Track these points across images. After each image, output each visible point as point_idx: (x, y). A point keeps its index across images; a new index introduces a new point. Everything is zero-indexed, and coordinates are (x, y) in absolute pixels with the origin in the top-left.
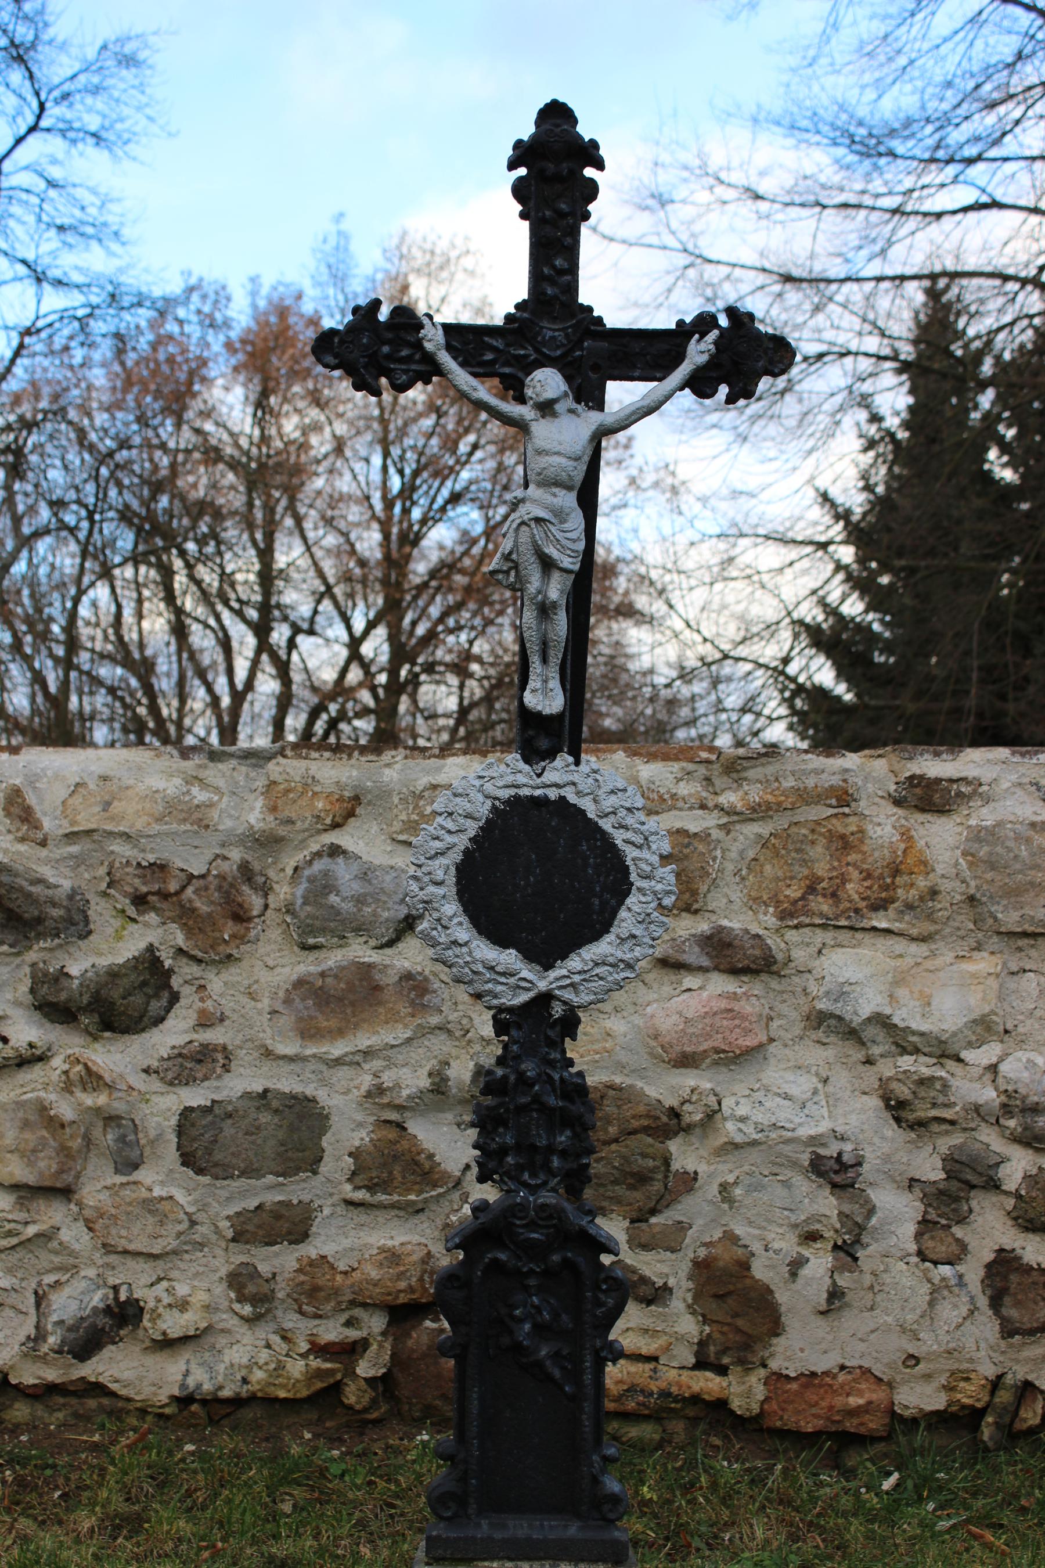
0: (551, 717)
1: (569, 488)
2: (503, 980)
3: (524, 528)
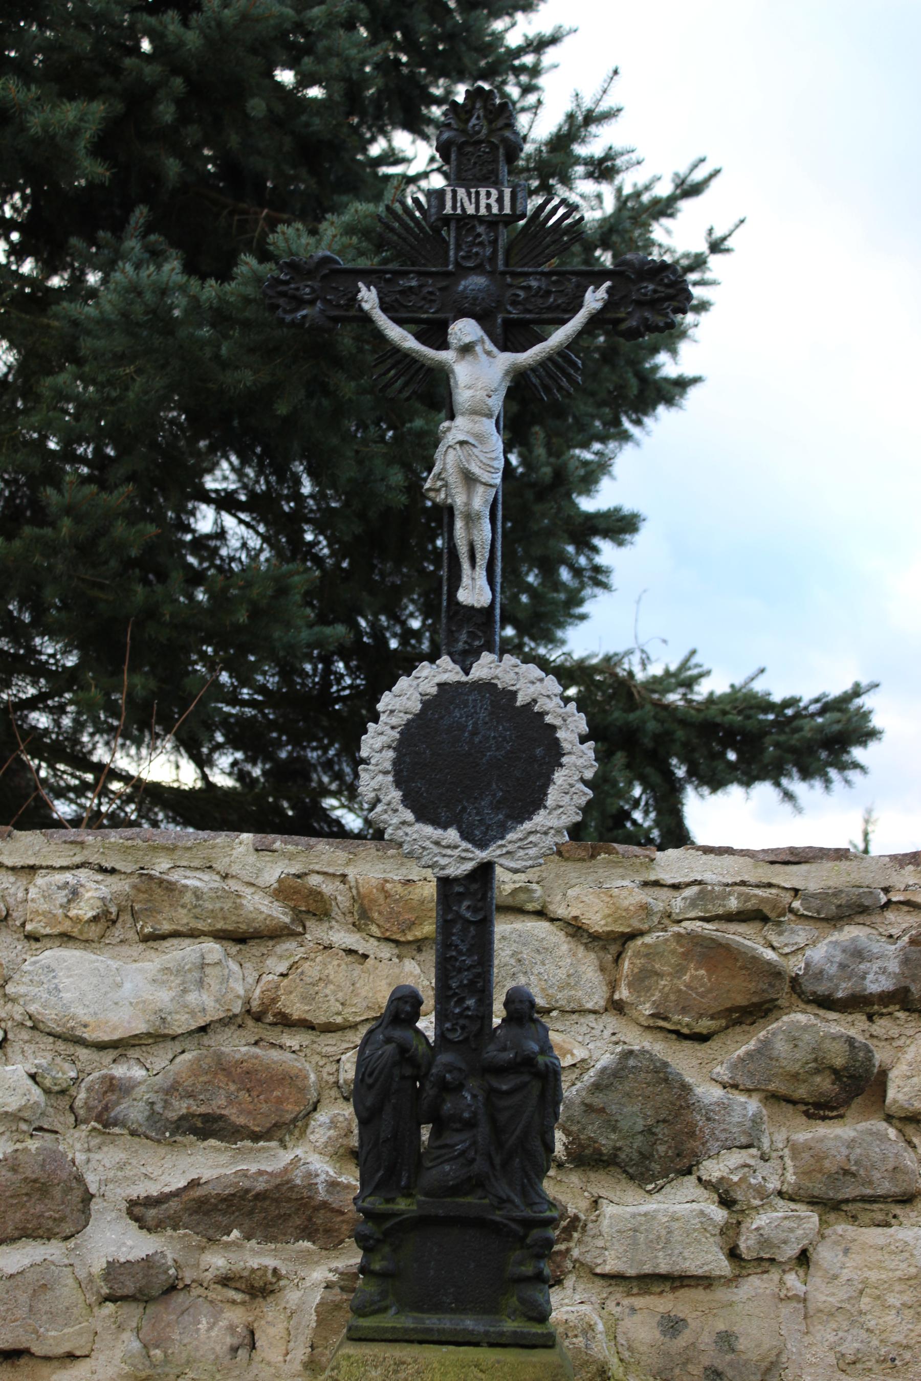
0: (482, 610)
1: (489, 416)
2: (449, 852)
3: (451, 450)
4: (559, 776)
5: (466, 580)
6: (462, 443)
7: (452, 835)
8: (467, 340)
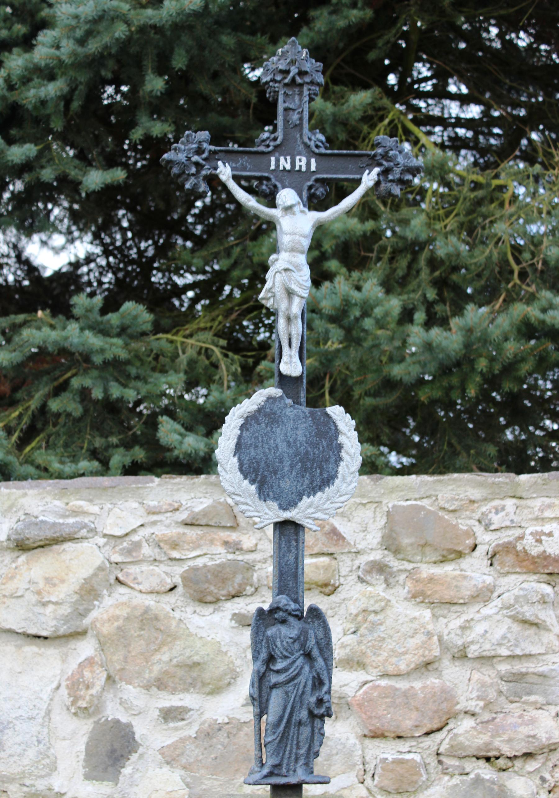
1: (302, 253)
5: (285, 358)
6: (286, 270)
8: (289, 203)
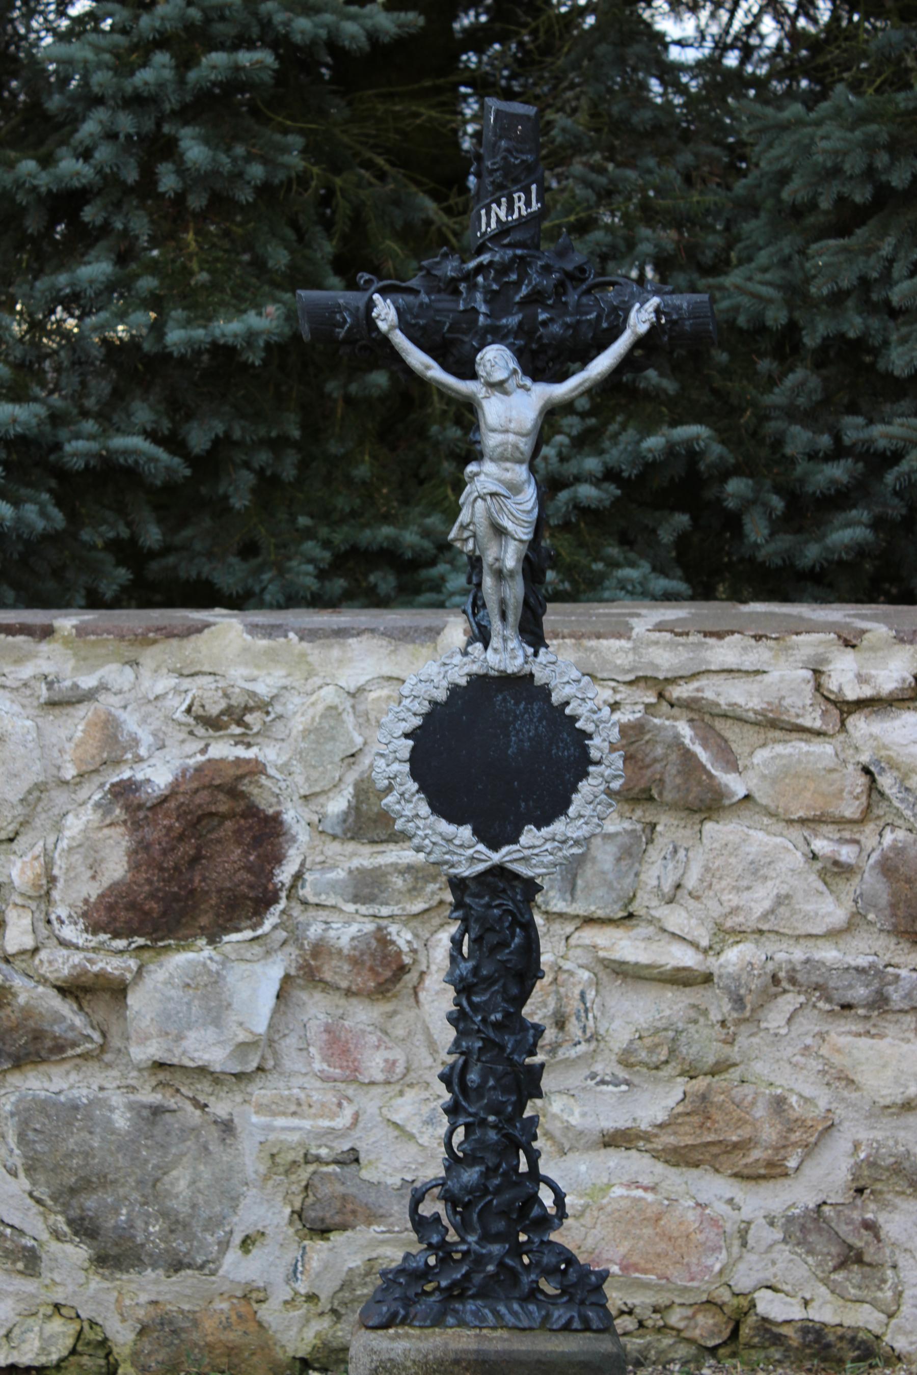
1: (520, 462)
4: (586, 787)
6: (493, 495)
7: (466, 832)
